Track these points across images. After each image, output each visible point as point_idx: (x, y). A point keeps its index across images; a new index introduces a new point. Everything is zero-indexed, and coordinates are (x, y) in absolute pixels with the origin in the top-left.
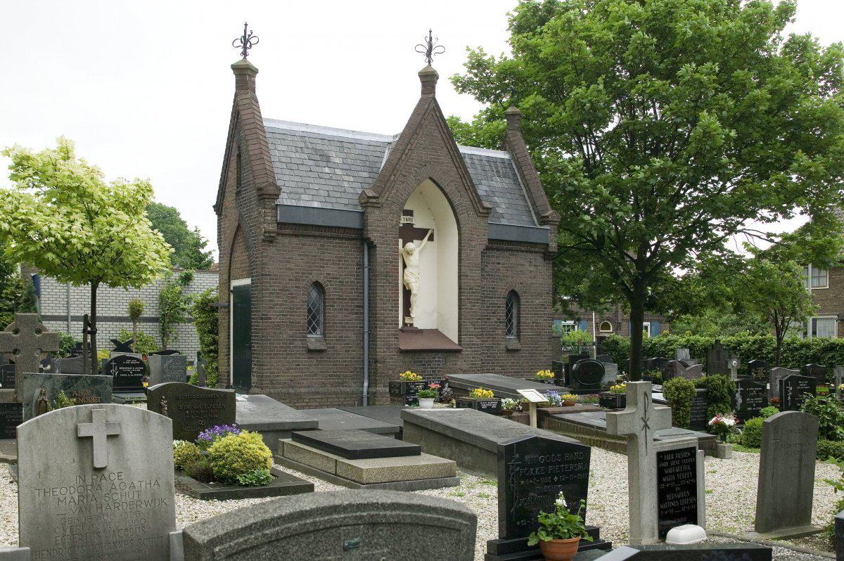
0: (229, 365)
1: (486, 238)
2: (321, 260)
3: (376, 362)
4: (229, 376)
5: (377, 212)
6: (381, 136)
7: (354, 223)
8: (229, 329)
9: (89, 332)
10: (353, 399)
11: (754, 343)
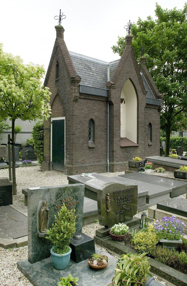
0: (50, 154)
1: (146, 103)
2: (93, 109)
3: (113, 152)
4: (50, 158)
5: (114, 90)
6: (105, 62)
7: (104, 94)
8: (50, 138)
9: (11, 144)
10: (104, 167)
11: (180, 139)
